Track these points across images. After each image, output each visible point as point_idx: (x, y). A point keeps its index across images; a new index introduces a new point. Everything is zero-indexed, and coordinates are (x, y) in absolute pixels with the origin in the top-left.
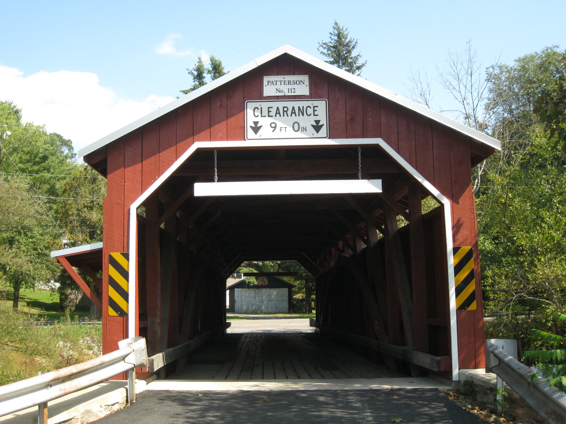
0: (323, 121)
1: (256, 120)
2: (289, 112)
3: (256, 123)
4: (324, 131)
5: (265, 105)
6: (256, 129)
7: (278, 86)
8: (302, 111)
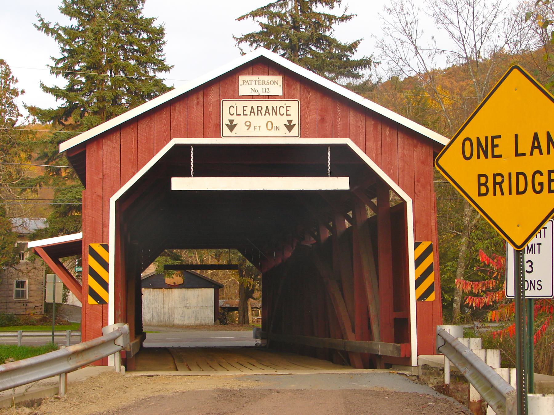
1: (231, 118)
2: (263, 112)
3: (231, 121)
4: (296, 131)
5: (240, 104)
7: (253, 86)
8: (275, 111)
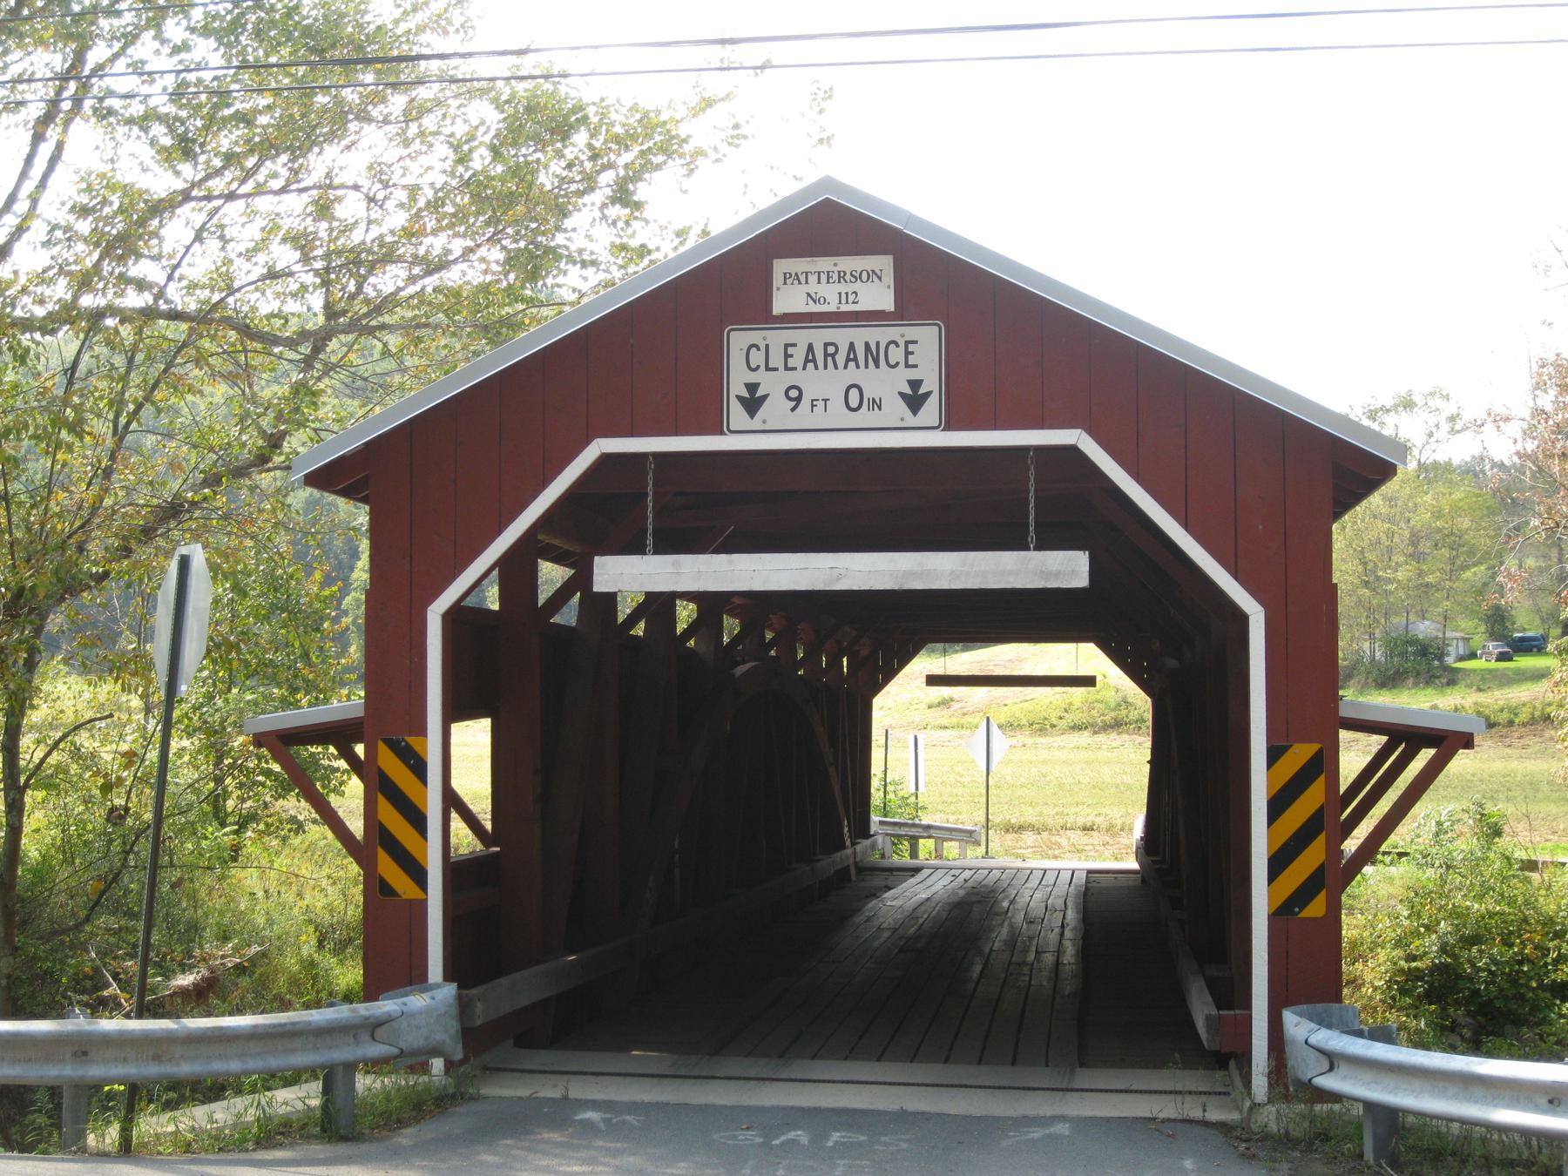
0: (931, 382)
1: (752, 378)
2: (841, 359)
4: (931, 411)
5: (776, 338)
6: (753, 403)
8: (874, 356)
